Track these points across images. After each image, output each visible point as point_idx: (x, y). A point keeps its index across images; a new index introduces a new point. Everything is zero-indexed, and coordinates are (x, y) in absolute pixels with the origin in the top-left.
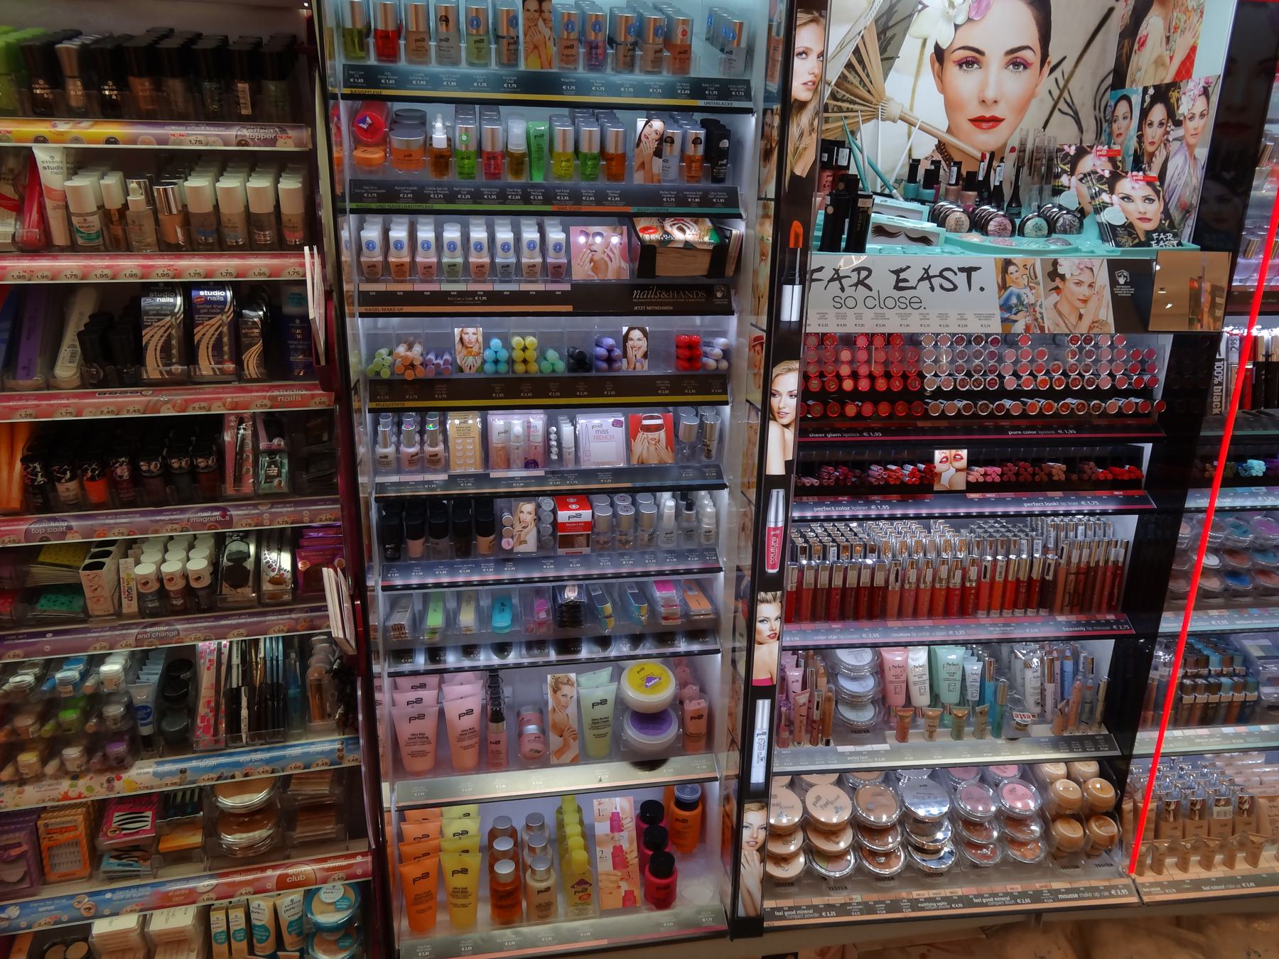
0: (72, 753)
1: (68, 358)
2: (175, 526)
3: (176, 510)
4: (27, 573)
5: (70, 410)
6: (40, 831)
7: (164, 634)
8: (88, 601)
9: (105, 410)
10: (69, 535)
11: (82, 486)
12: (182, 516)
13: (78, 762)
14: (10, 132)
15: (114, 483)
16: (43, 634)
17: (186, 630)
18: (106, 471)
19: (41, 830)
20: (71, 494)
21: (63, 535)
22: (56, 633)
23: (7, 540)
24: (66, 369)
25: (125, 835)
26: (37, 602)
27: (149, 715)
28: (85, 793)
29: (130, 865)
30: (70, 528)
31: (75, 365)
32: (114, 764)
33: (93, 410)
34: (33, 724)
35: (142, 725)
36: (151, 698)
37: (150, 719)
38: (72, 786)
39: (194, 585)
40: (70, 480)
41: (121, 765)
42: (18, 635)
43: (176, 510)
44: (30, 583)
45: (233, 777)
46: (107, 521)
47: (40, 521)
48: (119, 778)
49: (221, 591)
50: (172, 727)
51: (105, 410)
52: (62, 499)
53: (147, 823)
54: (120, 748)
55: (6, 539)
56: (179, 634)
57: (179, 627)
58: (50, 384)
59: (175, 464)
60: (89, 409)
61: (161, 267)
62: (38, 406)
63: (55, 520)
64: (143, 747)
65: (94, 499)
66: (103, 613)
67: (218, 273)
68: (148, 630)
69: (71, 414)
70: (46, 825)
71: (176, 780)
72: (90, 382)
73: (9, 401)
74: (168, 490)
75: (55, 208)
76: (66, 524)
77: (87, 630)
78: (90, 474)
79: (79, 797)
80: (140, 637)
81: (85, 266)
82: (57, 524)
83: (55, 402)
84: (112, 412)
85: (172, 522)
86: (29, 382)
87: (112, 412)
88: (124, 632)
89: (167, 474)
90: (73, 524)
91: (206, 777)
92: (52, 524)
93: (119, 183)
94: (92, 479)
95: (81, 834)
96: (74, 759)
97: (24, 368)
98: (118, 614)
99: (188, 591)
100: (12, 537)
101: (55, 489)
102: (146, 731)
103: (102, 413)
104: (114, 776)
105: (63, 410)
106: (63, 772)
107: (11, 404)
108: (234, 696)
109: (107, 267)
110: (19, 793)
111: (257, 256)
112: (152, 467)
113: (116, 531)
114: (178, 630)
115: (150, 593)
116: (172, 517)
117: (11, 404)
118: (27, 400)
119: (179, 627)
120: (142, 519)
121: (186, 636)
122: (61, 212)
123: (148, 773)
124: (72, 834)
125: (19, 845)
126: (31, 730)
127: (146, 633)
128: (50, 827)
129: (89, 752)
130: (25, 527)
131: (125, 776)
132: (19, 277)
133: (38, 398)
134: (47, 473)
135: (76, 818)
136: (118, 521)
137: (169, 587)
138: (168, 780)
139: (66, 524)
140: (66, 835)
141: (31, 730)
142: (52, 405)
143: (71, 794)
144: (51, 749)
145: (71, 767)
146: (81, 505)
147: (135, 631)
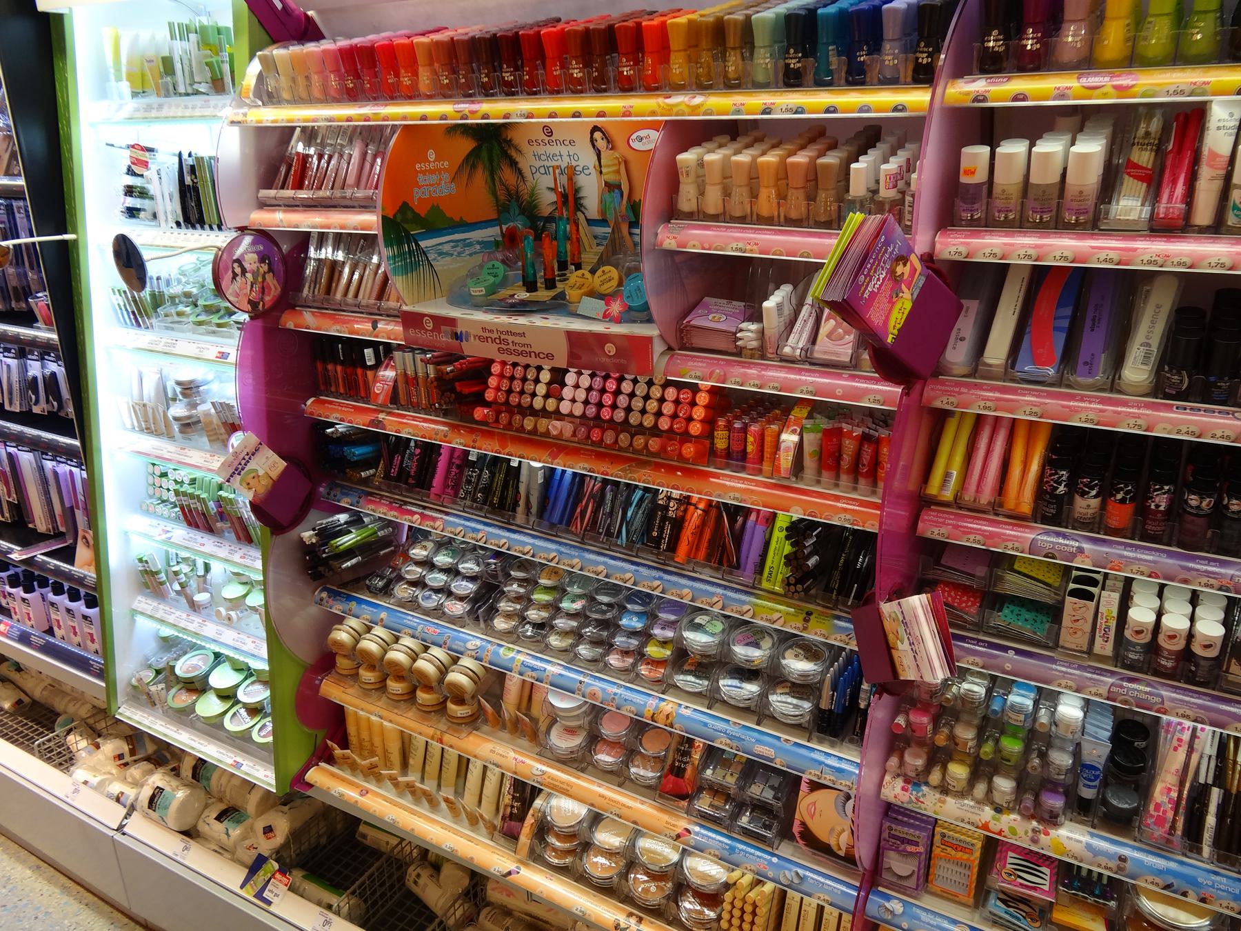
0: (1004, 785)
1: (1140, 359)
2: (1212, 581)
3: (1215, 560)
4: (1001, 579)
5: (1140, 422)
6: (936, 839)
7: (1144, 697)
8: (1063, 630)
9: (1184, 429)
10: (1079, 559)
11: (1103, 506)
12: (1222, 571)
13: (1008, 798)
14: (1208, 83)
15: (1143, 511)
16: (1005, 649)
17: (1173, 700)
18: (1140, 500)
19: (937, 838)
20: (1090, 511)
21: (1072, 557)
22: (1018, 652)
23: (1010, 545)
24: (1136, 372)
25: (1021, 884)
26: (1000, 610)
27: (1097, 777)
28: (1007, 832)
29: (1018, 919)
30: (1081, 550)
31: (1149, 368)
32: (1046, 816)
33: (1169, 427)
34: (972, 739)
35: (1085, 785)
36: (1103, 761)
37: (1097, 783)
38: (994, 818)
39: (1197, 649)
40: (1095, 497)
41: (1052, 820)
42: (979, 641)
43: (1215, 560)
44: (999, 589)
45: (1185, 894)
46: (1126, 553)
47: (1047, 533)
48: (1047, 834)
49: (1228, 667)
50: (1122, 803)
51: (1184, 429)
52: (1076, 515)
53: (1044, 880)
54: (1056, 802)
55: (1010, 545)
56: (1163, 703)
57: (1164, 693)
58: (1114, 384)
59: (1193, 500)
60: (1164, 425)
61: (1023, 246)
62: (1101, 411)
63: (1065, 536)
64: (1082, 809)
65: (1114, 523)
66: (1074, 647)
67: (1206, 262)
68: (1125, 684)
69: (1140, 427)
70: (943, 835)
71: (1113, 864)
72: (1160, 389)
73: (1070, 400)
74: (1209, 533)
75: (1213, 179)
76: (1077, 544)
77: (1051, 660)
78: (1119, 496)
79: (1000, 833)
80: (1114, 689)
81: (1005, 244)
82: (1066, 542)
83: (1124, 409)
84: (1193, 434)
85: (1208, 574)
86: (1090, 380)
87: (1193, 434)
88: (1095, 676)
89: (1177, 508)
90: (1087, 546)
91: (1150, 879)
92: (1061, 541)
93: (1104, 151)
94: (1123, 501)
95: (973, 861)
96: (1004, 792)
97: (1086, 363)
98: (1090, 652)
99: (1187, 655)
100: (1017, 545)
101: (1071, 502)
102: (1088, 793)
103: (1179, 432)
104: (1041, 827)
105: (1132, 421)
106: (988, 799)
107: (1071, 403)
108: (1199, 796)
109: (1030, 246)
110: (940, 801)
111: (1025, 234)
112: (1204, 504)
113: (1135, 568)
114: (1162, 697)
115: (1138, 644)
116: (1210, 569)
117: (1071, 403)
118: (1090, 402)
119: (1164, 693)
120: (1171, 561)
121: (1173, 708)
122: (1218, 185)
123: (1080, 842)
124: (966, 856)
125: (916, 844)
126: (970, 744)
127: (1122, 687)
128: (946, 839)
129: (1020, 788)
130: (1032, 536)
131: (1053, 832)
132: (1149, 262)
133: (1103, 401)
134: (1071, 484)
135: (975, 841)
136: (1140, 556)
137: (1162, 640)
138: (1103, 861)
139: (1077, 544)
140: (960, 854)
141: (970, 744)
142: (1119, 413)
143: (991, 826)
144: (982, 770)
145: (998, 798)
146: (1096, 525)
147: (1110, 680)
